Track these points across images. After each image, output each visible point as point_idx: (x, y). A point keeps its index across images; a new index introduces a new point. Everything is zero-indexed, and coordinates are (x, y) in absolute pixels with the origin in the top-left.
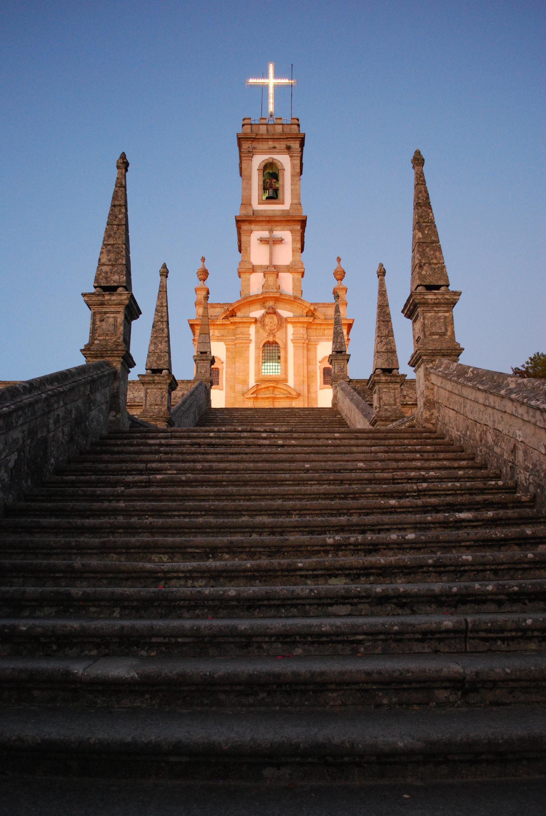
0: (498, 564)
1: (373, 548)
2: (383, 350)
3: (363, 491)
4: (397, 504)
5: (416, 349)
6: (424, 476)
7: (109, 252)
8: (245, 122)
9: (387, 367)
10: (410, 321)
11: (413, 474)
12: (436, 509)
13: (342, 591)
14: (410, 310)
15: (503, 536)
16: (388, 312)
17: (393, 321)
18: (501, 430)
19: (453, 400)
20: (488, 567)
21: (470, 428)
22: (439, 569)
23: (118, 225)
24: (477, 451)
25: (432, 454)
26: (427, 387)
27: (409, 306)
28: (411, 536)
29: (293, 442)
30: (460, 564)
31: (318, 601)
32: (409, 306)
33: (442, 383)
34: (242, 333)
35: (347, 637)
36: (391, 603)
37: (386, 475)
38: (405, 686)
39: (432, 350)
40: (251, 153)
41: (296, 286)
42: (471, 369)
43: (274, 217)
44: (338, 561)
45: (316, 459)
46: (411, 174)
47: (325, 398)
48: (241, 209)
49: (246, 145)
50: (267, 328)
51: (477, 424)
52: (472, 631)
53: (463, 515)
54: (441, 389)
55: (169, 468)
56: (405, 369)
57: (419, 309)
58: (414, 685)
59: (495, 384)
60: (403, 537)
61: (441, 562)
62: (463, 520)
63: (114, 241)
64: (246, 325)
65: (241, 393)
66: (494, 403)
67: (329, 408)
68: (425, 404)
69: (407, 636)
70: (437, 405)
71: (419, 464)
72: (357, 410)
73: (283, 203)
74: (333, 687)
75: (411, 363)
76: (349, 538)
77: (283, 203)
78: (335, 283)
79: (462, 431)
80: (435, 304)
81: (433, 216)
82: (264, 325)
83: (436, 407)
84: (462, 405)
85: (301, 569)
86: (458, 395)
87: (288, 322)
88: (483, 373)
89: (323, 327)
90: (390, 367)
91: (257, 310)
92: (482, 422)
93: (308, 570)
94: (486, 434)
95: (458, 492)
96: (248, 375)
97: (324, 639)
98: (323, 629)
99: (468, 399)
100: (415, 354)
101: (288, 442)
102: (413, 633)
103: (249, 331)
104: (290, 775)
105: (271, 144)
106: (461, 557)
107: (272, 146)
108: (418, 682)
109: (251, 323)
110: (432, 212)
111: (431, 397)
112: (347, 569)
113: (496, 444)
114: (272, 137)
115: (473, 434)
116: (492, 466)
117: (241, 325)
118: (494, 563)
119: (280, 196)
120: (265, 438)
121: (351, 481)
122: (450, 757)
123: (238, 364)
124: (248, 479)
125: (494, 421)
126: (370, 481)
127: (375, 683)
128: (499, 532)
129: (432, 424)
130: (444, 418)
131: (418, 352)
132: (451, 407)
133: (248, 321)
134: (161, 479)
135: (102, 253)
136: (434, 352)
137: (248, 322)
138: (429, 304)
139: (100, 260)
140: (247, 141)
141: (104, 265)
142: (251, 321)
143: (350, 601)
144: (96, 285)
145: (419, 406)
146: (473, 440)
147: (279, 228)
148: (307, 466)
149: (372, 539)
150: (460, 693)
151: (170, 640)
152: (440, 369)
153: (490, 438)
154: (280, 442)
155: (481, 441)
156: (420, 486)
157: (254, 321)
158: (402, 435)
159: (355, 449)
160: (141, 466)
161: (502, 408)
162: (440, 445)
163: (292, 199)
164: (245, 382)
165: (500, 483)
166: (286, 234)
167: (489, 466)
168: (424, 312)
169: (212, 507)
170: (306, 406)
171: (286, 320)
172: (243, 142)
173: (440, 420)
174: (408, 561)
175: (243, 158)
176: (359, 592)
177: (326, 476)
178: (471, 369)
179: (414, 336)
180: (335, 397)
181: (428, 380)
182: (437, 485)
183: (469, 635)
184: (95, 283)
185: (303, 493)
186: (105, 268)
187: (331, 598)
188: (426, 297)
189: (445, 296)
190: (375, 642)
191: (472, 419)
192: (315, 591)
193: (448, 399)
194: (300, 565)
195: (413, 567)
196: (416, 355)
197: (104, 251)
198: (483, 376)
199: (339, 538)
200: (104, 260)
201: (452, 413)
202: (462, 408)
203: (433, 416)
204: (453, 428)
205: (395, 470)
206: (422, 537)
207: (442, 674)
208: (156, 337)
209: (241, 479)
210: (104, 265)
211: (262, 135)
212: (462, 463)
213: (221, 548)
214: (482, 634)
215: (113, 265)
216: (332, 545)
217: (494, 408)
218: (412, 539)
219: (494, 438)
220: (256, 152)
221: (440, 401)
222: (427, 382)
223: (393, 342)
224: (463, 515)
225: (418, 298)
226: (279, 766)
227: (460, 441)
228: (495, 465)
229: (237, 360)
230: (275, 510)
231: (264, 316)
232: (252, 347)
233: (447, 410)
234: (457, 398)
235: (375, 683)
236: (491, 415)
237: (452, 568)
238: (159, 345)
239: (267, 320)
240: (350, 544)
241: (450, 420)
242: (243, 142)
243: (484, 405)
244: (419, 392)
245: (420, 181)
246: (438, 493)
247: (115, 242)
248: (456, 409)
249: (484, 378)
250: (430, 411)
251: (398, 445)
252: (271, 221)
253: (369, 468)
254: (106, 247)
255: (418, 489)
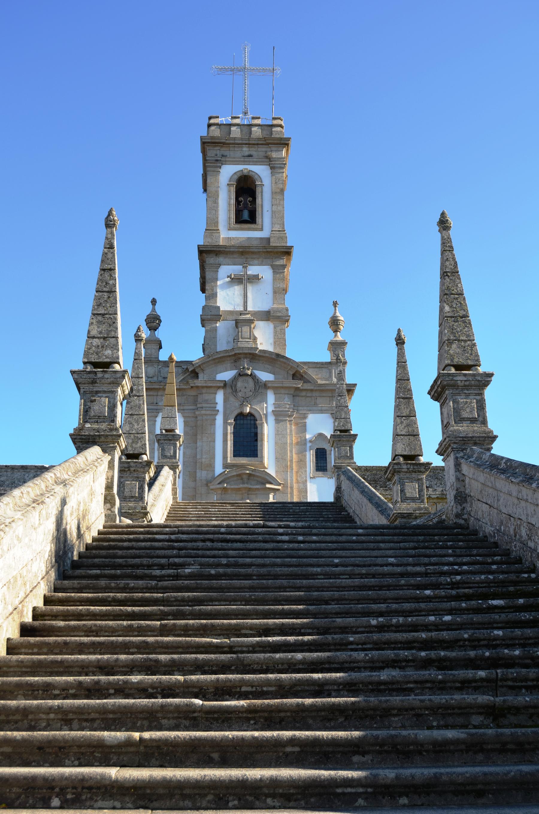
0: (526, 639)
1: (415, 628)
2: (403, 433)
3: (397, 583)
4: (432, 593)
5: (445, 436)
6: (457, 570)
7: (99, 322)
8: (212, 121)
9: (409, 453)
10: (437, 404)
11: (446, 568)
12: (468, 597)
13: (392, 655)
14: (437, 392)
15: (531, 618)
16: (409, 387)
17: (414, 397)
18: (534, 523)
19: (486, 493)
20: (517, 642)
21: (504, 522)
22: (473, 644)
23: (108, 292)
24: (511, 547)
25: (465, 550)
26: (458, 479)
27: (436, 387)
28: (448, 618)
29: (315, 538)
30: (492, 638)
31: (371, 665)
32: (436, 387)
33: (474, 474)
34: (206, 401)
35: (400, 685)
36: (433, 666)
37: (418, 569)
38: (449, 711)
39: (463, 437)
40: (219, 162)
41: (280, 339)
42: (504, 461)
43: (249, 247)
44: (385, 636)
45: (344, 554)
46: (437, 238)
47: (319, 490)
48: (205, 237)
49: (212, 152)
50: (240, 394)
51: (512, 518)
52: (501, 680)
53: (495, 602)
54: (473, 481)
55: (192, 562)
56: (430, 455)
57: (447, 392)
58: (456, 711)
59: (528, 476)
60: (441, 619)
61: (475, 637)
62: (496, 607)
63: (105, 310)
64: (212, 390)
65: (205, 482)
66: (527, 496)
67: (331, 503)
68: (455, 497)
69: (449, 684)
70: (469, 499)
71: (451, 559)
72: (370, 505)
73: (262, 229)
74: (395, 712)
75: (439, 451)
76: (391, 620)
77: (262, 229)
78: (330, 336)
79: (496, 526)
80: (465, 386)
81: (462, 287)
82: (235, 391)
83: (468, 501)
84: (496, 498)
85: (351, 643)
86: (491, 488)
87: (269, 388)
88: (516, 465)
89: (314, 394)
90: (413, 453)
91: (226, 370)
92: (516, 516)
93: (358, 645)
94: (520, 529)
95: (491, 585)
96: (213, 457)
97: (382, 687)
98: (382, 678)
99: (501, 491)
100: (444, 442)
101: (308, 538)
102: (454, 682)
103: (215, 398)
104: (372, 761)
105: (246, 150)
106: (493, 632)
107: (247, 153)
108: (460, 708)
109: (219, 388)
110: (460, 283)
111: (462, 489)
112: (392, 643)
113: (530, 538)
114: (247, 142)
115: (507, 529)
116: (526, 560)
117: (204, 391)
118: (522, 637)
119: (259, 220)
120: (282, 534)
121: (384, 575)
122: (485, 747)
123: (199, 444)
124: (279, 573)
125: (527, 515)
126: (402, 575)
127: (427, 709)
128: (528, 614)
129: (463, 519)
130: (476, 512)
131: (447, 440)
132: (484, 501)
133: (214, 385)
134: (189, 573)
135: (91, 324)
136: (465, 439)
137: (215, 387)
138: (458, 386)
139: (89, 332)
140: (215, 148)
141: (94, 337)
142: (218, 385)
143: (399, 664)
144: (86, 360)
145: (449, 500)
146: (508, 536)
147: (256, 262)
148: (336, 561)
149: (412, 620)
150: (491, 718)
151: (256, 689)
152: (472, 459)
153: (524, 532)
154: (300, 538)
155: (515, 536)
156: (454, 578)
157: (222, 385)
158: (431, 531)
159: (382, 545)
160: (163, 561)
161: (535, 501)
162: (473, 541)
163: (273, 224)
164: (211, 466)
165: (533, 576)
166: (264, 271)
167: (523, 561)
168: (454, 394)
169: (253, 597)
170: (295, 500)
171: (265, 386)
172: (208, 148)
173: (473, 515)
174: (446, 636)
175: (208, 169)
176: (406, 656)
177: (357, 570)
178: (504, 461)
179: (442, 421)
180: (338, 489)
181: (459, 471)
182: (471, 578)
183: (500, 683)
184: (84, 357)
185: (338, 585)
186: (96, 342)
187: (383, 662)
188: (455, 378)
189: (476, 378)
190: (423, 690)
191: (506, 513)
192: (370, 655)
193: (481, 491)
194: (351, 639)
195: (451, 641)
196: (445, 443)
197: (94, 321)
198: (516, 468)
199: (382, 620)
200: (94, 333)
201: (485, 507)
202: (496, 502)
203: (465, 511)
204: (487, 524)
205: (426, 565)
206: (458, 619)
207: (478, 701)
208: (131, 415)
209: (272, 573)
210: (94, 337)
211: (235, 139)
212: (495, 558)
213: (273, 629)
214: (510, 683)
215: (104, 338)
216: (375, 626)
217: (527, 501)
218: (449, 621)
219: (528, 533)
220: (226, 161)
221: (472, 494)
222: (458, 473)
223: (415, 423)
224: (495, 602)
225: (447, 379)
226: (363, 754)
227: (495, 537)
228: (530, 559)
229: (199, 437)
230: (314, 600)
231: (235, 379)
232: (219, 419)
233: (480, 504)
234: (491, 491)
235: (427, 709)
236: (524, 508)
237: (485, 642)
238: (136, 425)
239: (239, 384)
240: (392, 625)
241: (483, 515)
242: (208, 148)
243: (518, 499)
244: (448, 485)
245: (447, 248)
246: (471, 585)
247: (106, 312)
248: (489, 502)
249: (517, 470)
250: (461, 505)
251: (427, 542)
252: (244, 253)
253: (400, 563)
254: (96, 318)
255: (452, 581)
